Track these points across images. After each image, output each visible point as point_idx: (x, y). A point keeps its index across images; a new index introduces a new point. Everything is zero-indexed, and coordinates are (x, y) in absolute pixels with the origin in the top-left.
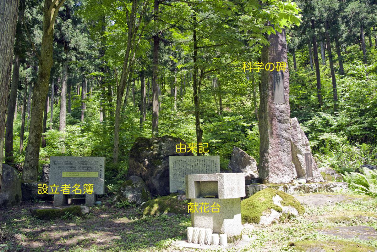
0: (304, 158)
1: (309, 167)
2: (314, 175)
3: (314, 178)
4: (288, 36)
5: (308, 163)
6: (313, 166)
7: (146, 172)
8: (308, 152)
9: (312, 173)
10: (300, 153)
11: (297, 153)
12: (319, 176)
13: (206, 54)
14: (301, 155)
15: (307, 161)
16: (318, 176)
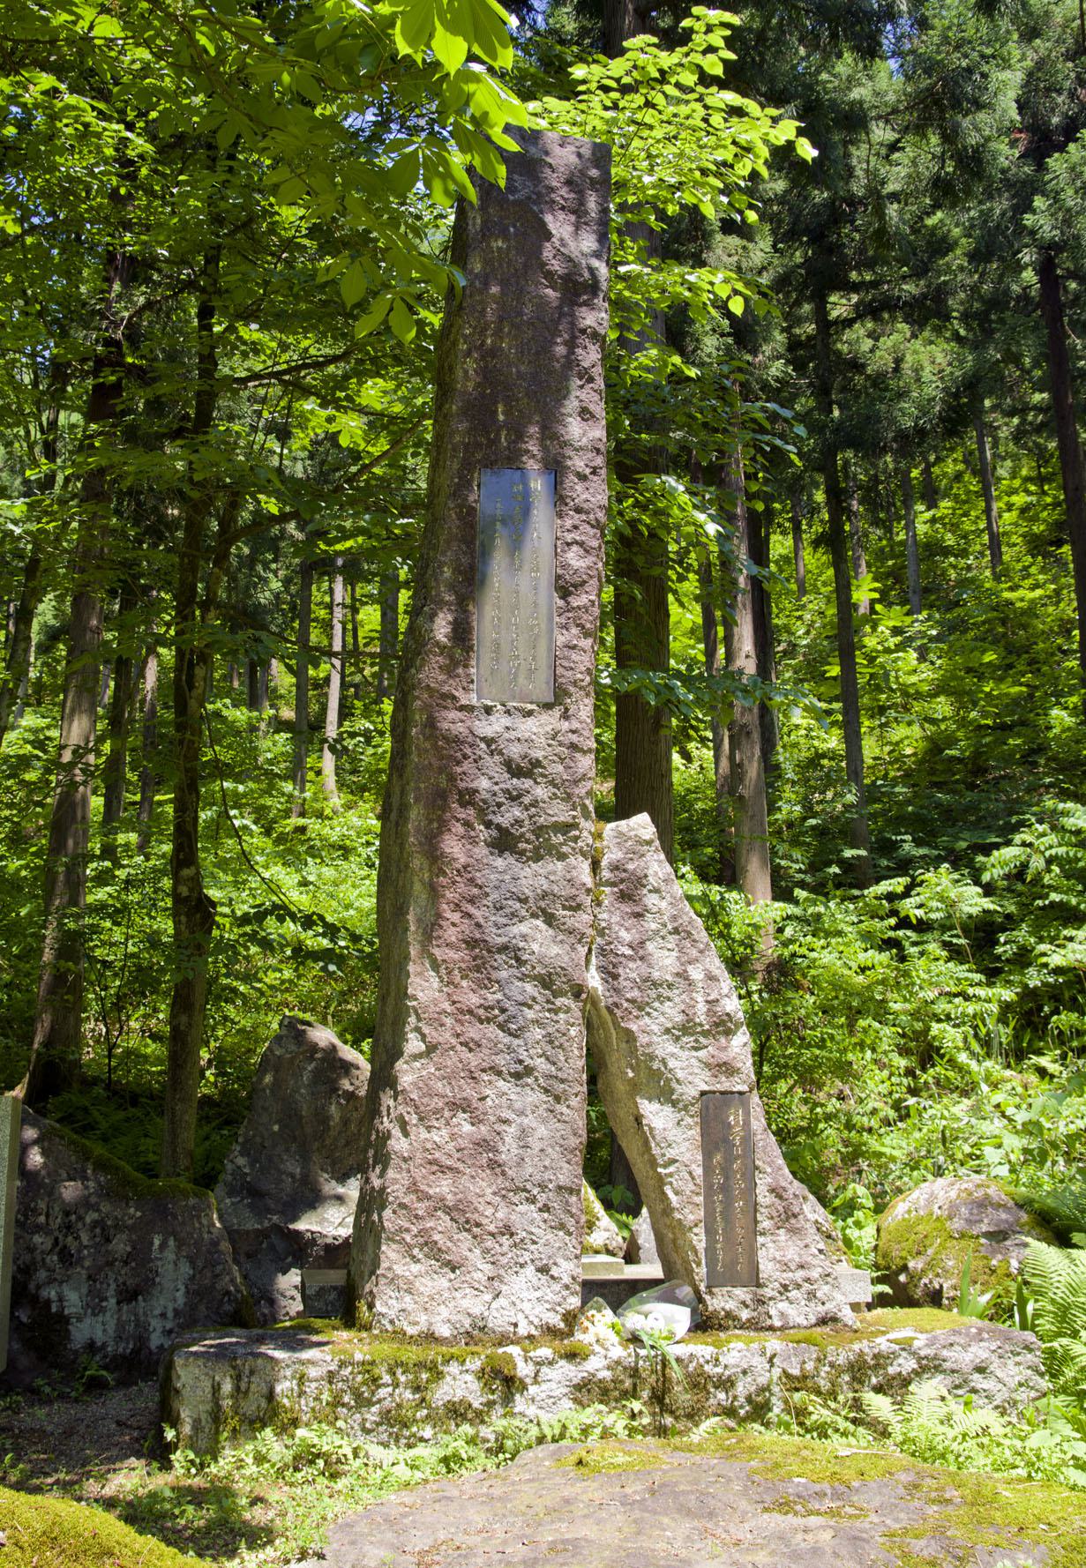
0: (695, 1133)
2: (767, 1268)
3: (768, 1292)
5: (726, 1171)
6: (764, 1197)
8: (724, 1084)
9: (752, 1252)
10: (665, 1094)
11: (635, 1088)
14: (668, 1109)
16: (800, 1274)
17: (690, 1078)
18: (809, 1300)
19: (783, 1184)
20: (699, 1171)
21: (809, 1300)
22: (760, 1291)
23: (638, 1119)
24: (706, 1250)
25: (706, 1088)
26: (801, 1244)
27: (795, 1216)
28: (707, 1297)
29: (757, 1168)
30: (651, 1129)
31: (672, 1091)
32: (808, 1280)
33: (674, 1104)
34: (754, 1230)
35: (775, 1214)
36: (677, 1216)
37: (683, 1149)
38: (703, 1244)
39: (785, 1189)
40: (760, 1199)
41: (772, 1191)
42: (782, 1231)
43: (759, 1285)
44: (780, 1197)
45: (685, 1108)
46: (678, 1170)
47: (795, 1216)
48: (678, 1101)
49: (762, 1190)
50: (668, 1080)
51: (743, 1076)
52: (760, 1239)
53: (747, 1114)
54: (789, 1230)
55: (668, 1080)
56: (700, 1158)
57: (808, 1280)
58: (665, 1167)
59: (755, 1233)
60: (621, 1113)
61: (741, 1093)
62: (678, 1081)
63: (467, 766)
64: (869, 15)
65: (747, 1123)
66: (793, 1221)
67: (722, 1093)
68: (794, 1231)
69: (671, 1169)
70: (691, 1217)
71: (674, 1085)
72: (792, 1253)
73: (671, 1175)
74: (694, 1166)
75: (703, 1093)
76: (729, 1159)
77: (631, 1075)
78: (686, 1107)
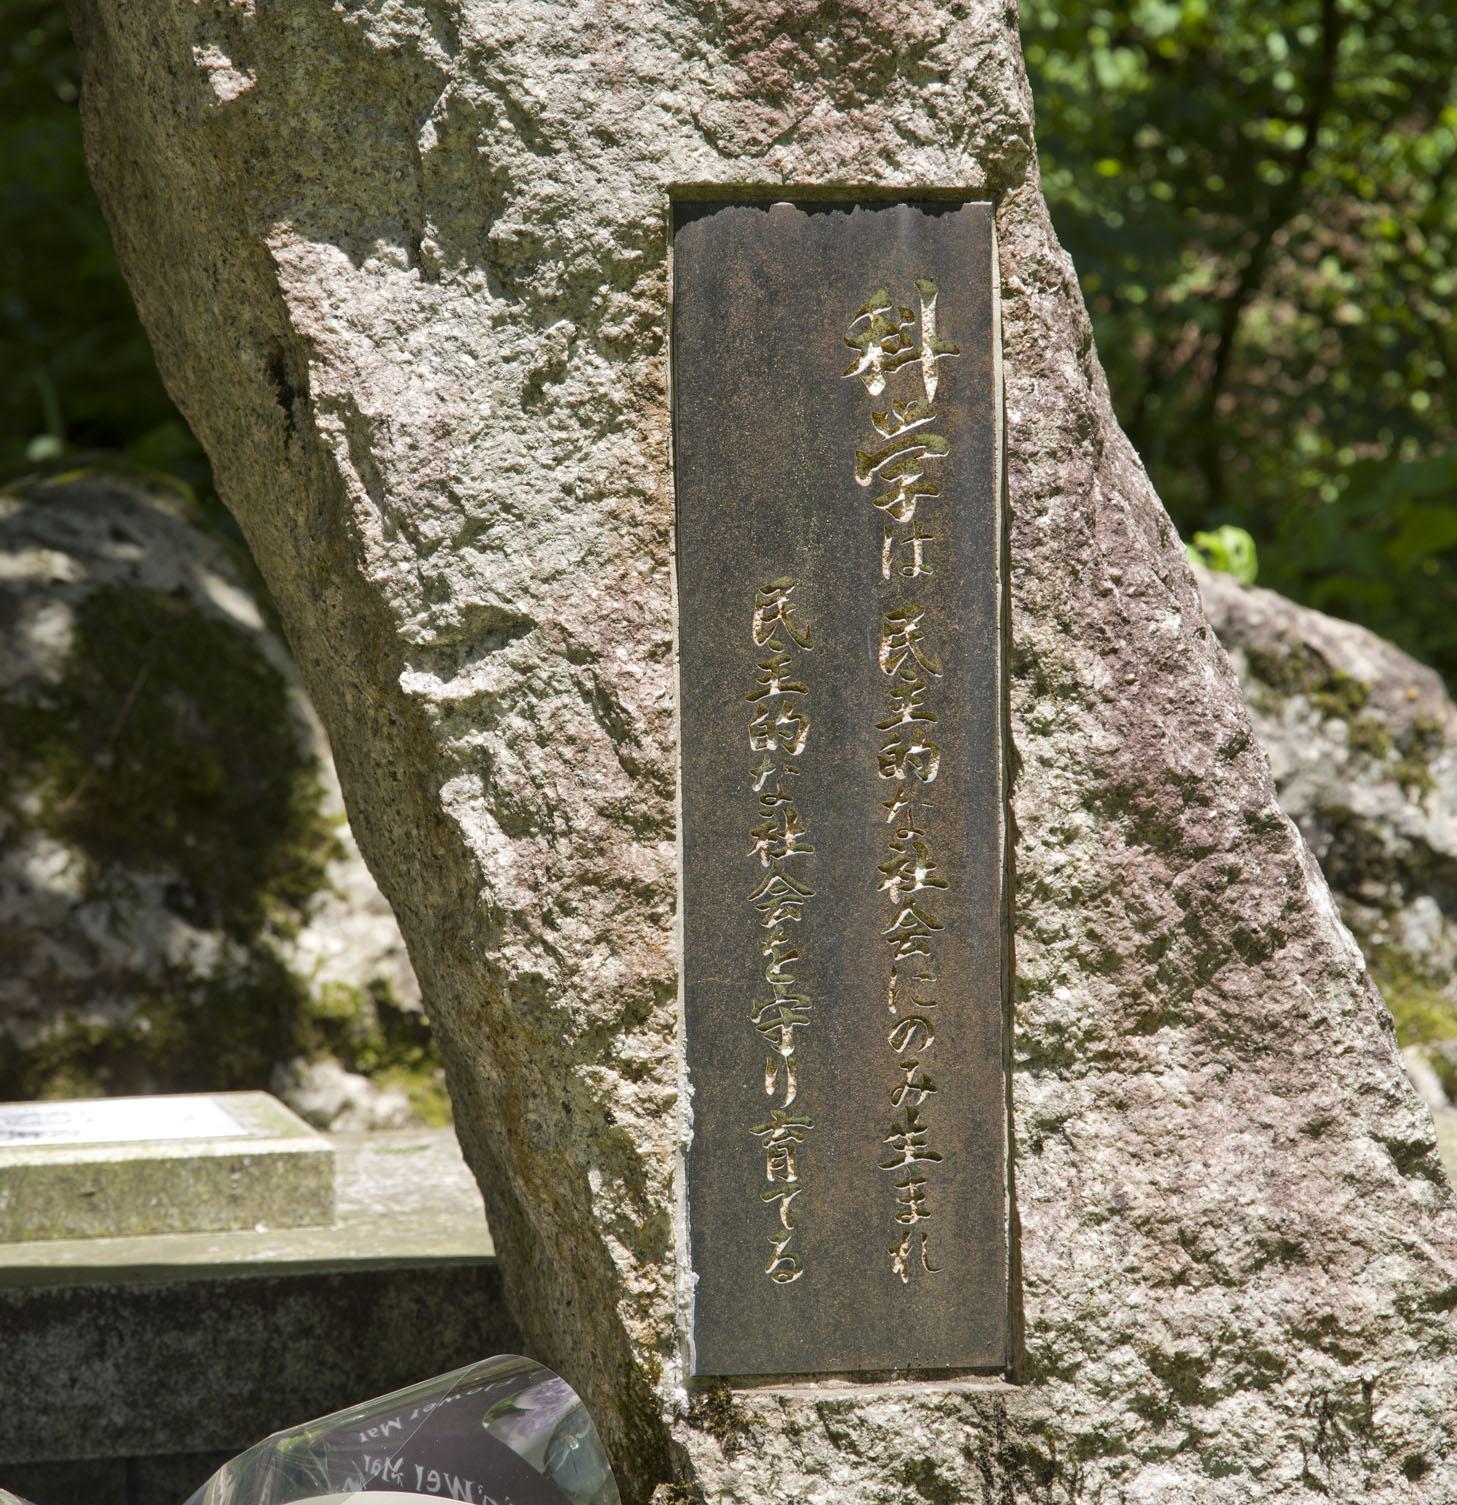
0: (639, 450)
1: (835, 888)
2: (1066, 1259)
3: (1075, 1407)
4: (285, 132)
5: (829, 688)
6: (1056, 833)
7: (133, 116)
8: (831, 145)
9: (982, 1165)
10: (448, 206)
11: (262, 173)
12: (1366, 1296)
13: (357, 163)
14: (469, 304)
15: (777, 606)
16: (1277, 1296)
17: (609, 106)
18: (1327, 1448)
19: (1185, 758)
20: (654, 687)
21: (1327, 1448)
22: (1026, 1404)
23: (287, 360)
24: (695, 1157)
25: (709, 168)
26: (1289, 1116)
27: (1254, 949)
28: (700, 1445)
29: (1022, 663)
30: (363, 430)
31: (495, 191)
32: (1321, 1331)
33: (507, 270)
34: (996, 1036)
35: (1127, 941)
36: (519, 958)
37: (559, 555)
38: (679, 1127)
39: (1191, 789)
40: (1038, 855)
41: (1112, 799)
42: (1170, 1042)
43: (1023, 1370)
44: (1163, 838)
45: (576, 300)
46: (527, 686)
47: (1254, 949)
48: (529, 253)
49: (1044, 793)
50: (466, 122)
51: (951, 96)
52: (1035, 1094)
53: (970, 332)
54: (1213, 1037)
55: (466, 122)
56: (664, 603)
57: (1321, 1331)
58: (447, 662)
59: (1004, 1053)
60: (197, 327)
61: (931, 201)
62: (528, 124)
63: (1280, 1267)
64: (447, 5)
65: (967, 385)
66: (1240, 979)
67: (815, 201)
68: (1242, 1040)
69: (484, 676)
70: (604, 968)
71: (505, 151)
72: (1229, 1168)
73: (480, 711)
74: (624, 658)
75: (690, 204)
76: (851, 607)
77: (228, 84)
78: (579, 287)
